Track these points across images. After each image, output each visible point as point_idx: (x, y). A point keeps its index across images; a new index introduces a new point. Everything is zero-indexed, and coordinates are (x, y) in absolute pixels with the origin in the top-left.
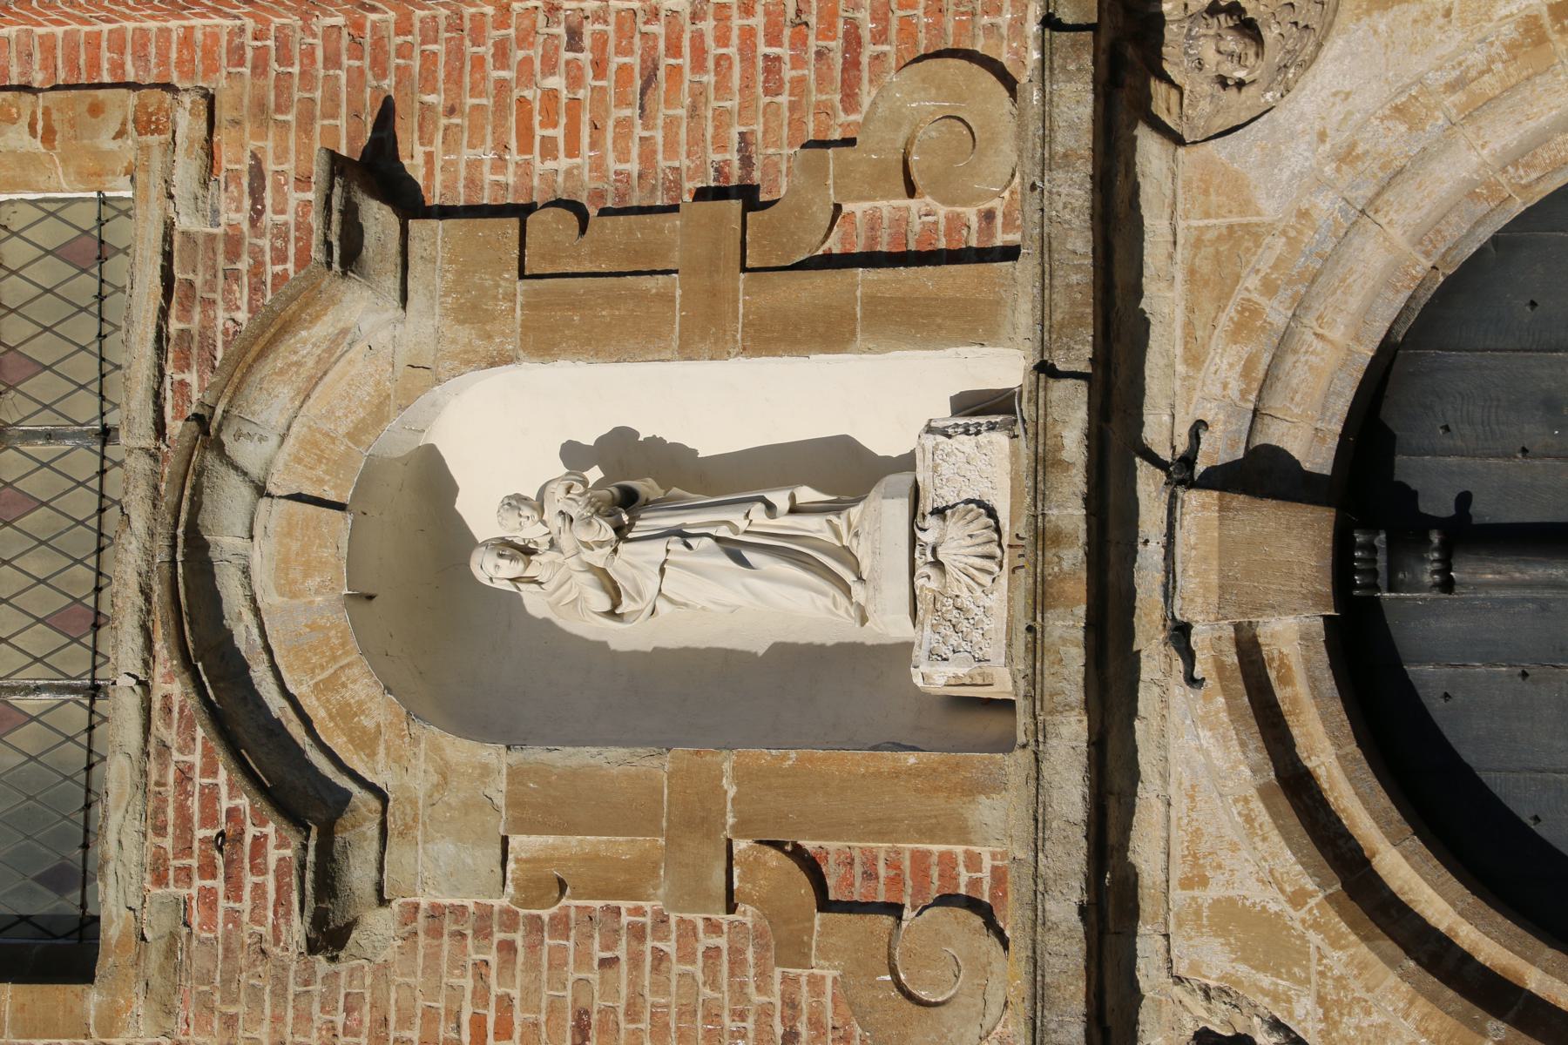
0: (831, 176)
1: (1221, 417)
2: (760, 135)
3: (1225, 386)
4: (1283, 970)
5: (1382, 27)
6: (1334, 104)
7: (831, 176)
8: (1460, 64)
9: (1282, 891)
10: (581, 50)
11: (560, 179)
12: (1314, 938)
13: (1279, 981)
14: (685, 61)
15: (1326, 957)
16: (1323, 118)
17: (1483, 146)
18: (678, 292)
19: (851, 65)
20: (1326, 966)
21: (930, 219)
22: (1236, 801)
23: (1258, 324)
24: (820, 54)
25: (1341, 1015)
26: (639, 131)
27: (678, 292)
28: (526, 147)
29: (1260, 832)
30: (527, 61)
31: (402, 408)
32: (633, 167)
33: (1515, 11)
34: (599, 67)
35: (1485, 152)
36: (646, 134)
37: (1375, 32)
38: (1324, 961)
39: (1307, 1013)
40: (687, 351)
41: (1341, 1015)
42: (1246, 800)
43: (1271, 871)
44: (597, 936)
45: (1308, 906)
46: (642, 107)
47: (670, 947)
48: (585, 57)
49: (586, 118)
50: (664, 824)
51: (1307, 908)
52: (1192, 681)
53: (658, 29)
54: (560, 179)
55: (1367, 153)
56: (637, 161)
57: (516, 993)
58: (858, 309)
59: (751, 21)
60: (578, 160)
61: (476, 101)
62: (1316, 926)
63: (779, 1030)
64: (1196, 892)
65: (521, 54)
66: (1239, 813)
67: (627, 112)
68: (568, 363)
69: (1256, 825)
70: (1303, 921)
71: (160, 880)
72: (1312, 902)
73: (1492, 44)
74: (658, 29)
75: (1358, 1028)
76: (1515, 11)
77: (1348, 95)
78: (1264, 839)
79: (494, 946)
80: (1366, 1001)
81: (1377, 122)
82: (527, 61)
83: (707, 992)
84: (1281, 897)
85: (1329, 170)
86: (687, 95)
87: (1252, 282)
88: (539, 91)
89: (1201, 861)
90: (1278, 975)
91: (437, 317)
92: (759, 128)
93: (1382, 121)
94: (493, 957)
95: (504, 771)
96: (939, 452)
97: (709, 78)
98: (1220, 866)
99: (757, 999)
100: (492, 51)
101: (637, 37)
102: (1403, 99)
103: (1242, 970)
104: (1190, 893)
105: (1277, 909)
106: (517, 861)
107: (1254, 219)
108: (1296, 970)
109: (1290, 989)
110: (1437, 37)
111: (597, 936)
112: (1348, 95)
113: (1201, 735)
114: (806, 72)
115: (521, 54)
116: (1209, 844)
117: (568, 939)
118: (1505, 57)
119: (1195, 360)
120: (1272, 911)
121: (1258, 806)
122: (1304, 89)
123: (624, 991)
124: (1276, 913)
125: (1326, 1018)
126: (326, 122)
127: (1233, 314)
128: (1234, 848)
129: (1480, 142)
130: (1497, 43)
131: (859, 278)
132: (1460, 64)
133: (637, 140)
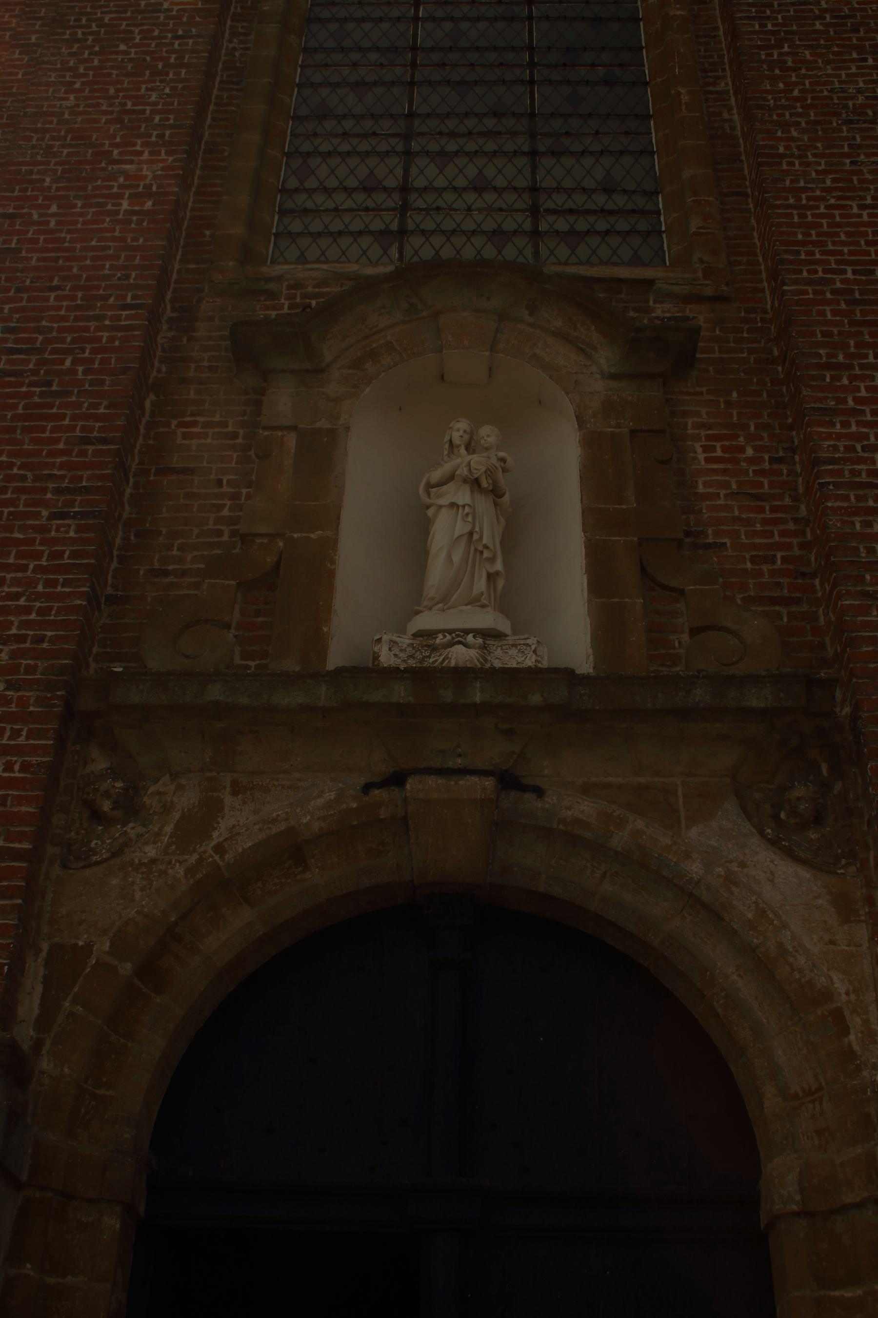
0: (701, 587)
1: (547, 806)
2: (725, 553)
3: (569, 808)
4: (174, 840)
5: (820, 901)
6: (765, 872)
7: (701, 587)
8: (797, 951)
9: (226, 840)
10: (770, 463)
11: (691, 455)
12: (194, 858)
13: (167, 837)
14: (768, 515)
15: (180, 865)
16: (755, 866)
17: (739, 976)
18: (624, 507)
19: (774, 601)
20: (175, 865)
21: (677, 644)
22: (287, 813)
23: (612, 828)
24: (779, 584)
25: (143, 873)
26: (723, 493)
27: (624, 507)
28: (708, 438)
29: (265, 827)
30: (761, 438)
31: (551, 377)
32: (701, 489)
33: (836, 986)
34: (762, 473)
35: (735, 977)
36: (722, 496)
37: (816, 898)
38: (178, 864)
39: (145, 853)
40: (586, 512)
41: (143, 873)
42: (287, 819)
43: (239, 834)
44: (237, 477)
45: (214, 855)
46: (737, 493)
47: (226, 512)
48: (766, 465)
49: (729, 466)
50: (297, 503)
51: (213, 854)
52: (367, 788)
53: (787, 501)
54: (691, 455)
55: (732, 893)
56: (705, 491)
57: (209, 441)
58: (617, 600)
59: (796, 549)
60: (703, 463)
61: (735, 415)
62: (201, 860)
63: (170, 568)
64: (228, 789)
65: (765, 435)
66: (278, 815)
67: (734, 486)
68: (579, 453)
69: (270, 825)
70: (205, 852)
71: (290, 287)
72: (217, 858)
73: (812, 971)
74: (787, 501)
75: (133, 883)
76: (836, 986)
77: (772, 881)
78: (260, 830)
79: (236, 430)
80: (150, 888)
81: (753, 899)
82: (761, 438)
83: (196, 531)
84: (221, 839)
85: (720, 870)
86: (747, 515)
87: (640, 824)
88: (743, 444)
89: (248, 792)
90: (171, 837)
91: (605, 392)
92: (730, 552)
93: (754, 902)
94: (230, 429)
95: (334, 427)
96: (525, 647)
97: (758, 527)
98: (244, 803)
99: (189, 558)
100: (765, 421)
101: (781, 491)
102: (770, 916)
103: (177, 815)
104: (228, 785)
105: (214, 837)
106: (283, 436)
107: (683, 825)
108: (174, 847)
109: (161, 843)
110: (814, 936)
111: (237, 477)
112: (772, 881)
113: (332, 793)
114: (767, 577)
115: (765, 435)
116: (260, 797)
117: (236, 463)
118: (803, 980)
119: (586, 790)
120: (213, 833)
121: (283, 826)
122: (775, 854)
123: (204, 491)
124: (212, 836)
125: (141, 864)
126: (716, 348)
127: (617, 813)
128: (256, 812)
129: (742, 973)
130: (813, 975)
131: (636, 600)
132: (797, 951)
133: (718, 491)
